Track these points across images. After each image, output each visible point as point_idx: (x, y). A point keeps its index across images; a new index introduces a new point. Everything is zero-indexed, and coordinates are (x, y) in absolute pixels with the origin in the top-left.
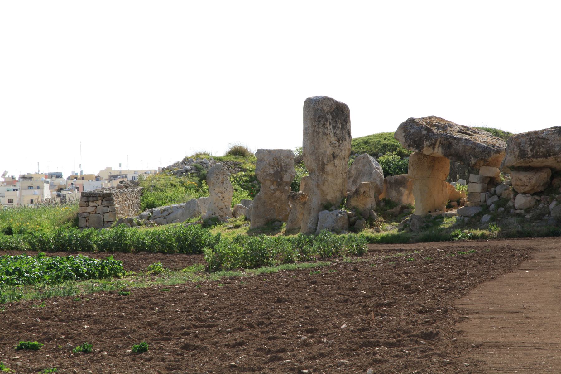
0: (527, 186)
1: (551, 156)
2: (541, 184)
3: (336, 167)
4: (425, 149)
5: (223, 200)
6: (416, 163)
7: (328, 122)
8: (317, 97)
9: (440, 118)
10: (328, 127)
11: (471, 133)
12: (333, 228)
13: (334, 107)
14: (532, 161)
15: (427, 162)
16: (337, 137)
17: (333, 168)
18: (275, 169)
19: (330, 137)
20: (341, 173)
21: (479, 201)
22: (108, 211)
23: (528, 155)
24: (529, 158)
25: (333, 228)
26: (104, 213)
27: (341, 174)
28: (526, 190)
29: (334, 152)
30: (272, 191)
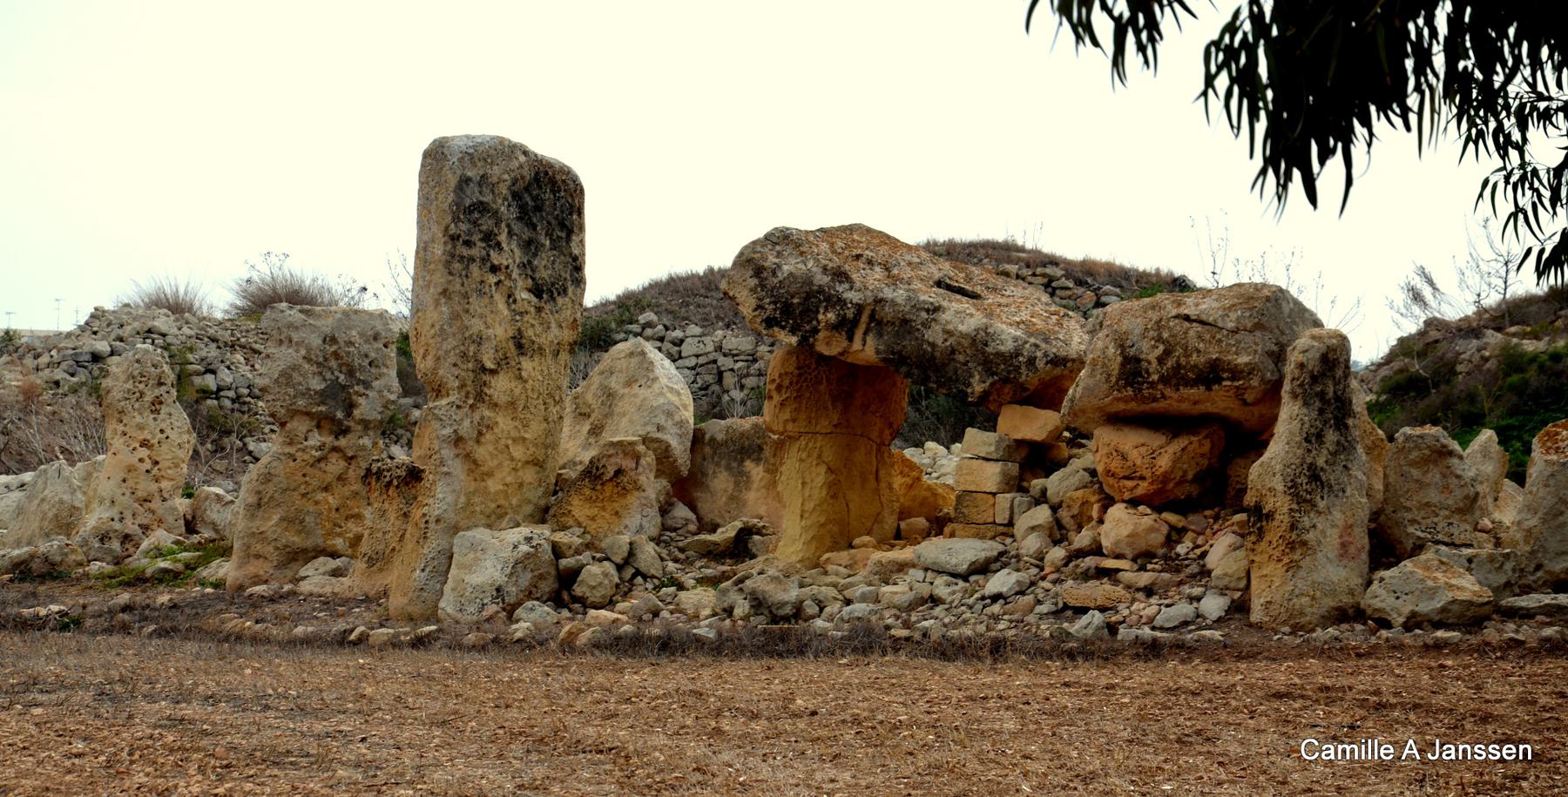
0: (1142, 478)
1: (1224, 383)
2: (1190, 476)
3: (526, 381)
4: (821, 335)
5: (155, 471)
6: (791, 383)
7: (503, 225)
8: (467, 137)
9: (881, 232)
10: (504, 245)
11: (978, 289)
12: (498, 590)
13: (527, 173)
15: (828, 380)
16: (533, 279)
17: (513, 384)
18: (328, 376)
19: (509, 276)
20: (541, 401)
21: (991, 520)
24: (1152, 385)
25: (498, 590)
27: (543, 407)
28: (1139, 491)
29: (519, 330)
30: (313, 452)
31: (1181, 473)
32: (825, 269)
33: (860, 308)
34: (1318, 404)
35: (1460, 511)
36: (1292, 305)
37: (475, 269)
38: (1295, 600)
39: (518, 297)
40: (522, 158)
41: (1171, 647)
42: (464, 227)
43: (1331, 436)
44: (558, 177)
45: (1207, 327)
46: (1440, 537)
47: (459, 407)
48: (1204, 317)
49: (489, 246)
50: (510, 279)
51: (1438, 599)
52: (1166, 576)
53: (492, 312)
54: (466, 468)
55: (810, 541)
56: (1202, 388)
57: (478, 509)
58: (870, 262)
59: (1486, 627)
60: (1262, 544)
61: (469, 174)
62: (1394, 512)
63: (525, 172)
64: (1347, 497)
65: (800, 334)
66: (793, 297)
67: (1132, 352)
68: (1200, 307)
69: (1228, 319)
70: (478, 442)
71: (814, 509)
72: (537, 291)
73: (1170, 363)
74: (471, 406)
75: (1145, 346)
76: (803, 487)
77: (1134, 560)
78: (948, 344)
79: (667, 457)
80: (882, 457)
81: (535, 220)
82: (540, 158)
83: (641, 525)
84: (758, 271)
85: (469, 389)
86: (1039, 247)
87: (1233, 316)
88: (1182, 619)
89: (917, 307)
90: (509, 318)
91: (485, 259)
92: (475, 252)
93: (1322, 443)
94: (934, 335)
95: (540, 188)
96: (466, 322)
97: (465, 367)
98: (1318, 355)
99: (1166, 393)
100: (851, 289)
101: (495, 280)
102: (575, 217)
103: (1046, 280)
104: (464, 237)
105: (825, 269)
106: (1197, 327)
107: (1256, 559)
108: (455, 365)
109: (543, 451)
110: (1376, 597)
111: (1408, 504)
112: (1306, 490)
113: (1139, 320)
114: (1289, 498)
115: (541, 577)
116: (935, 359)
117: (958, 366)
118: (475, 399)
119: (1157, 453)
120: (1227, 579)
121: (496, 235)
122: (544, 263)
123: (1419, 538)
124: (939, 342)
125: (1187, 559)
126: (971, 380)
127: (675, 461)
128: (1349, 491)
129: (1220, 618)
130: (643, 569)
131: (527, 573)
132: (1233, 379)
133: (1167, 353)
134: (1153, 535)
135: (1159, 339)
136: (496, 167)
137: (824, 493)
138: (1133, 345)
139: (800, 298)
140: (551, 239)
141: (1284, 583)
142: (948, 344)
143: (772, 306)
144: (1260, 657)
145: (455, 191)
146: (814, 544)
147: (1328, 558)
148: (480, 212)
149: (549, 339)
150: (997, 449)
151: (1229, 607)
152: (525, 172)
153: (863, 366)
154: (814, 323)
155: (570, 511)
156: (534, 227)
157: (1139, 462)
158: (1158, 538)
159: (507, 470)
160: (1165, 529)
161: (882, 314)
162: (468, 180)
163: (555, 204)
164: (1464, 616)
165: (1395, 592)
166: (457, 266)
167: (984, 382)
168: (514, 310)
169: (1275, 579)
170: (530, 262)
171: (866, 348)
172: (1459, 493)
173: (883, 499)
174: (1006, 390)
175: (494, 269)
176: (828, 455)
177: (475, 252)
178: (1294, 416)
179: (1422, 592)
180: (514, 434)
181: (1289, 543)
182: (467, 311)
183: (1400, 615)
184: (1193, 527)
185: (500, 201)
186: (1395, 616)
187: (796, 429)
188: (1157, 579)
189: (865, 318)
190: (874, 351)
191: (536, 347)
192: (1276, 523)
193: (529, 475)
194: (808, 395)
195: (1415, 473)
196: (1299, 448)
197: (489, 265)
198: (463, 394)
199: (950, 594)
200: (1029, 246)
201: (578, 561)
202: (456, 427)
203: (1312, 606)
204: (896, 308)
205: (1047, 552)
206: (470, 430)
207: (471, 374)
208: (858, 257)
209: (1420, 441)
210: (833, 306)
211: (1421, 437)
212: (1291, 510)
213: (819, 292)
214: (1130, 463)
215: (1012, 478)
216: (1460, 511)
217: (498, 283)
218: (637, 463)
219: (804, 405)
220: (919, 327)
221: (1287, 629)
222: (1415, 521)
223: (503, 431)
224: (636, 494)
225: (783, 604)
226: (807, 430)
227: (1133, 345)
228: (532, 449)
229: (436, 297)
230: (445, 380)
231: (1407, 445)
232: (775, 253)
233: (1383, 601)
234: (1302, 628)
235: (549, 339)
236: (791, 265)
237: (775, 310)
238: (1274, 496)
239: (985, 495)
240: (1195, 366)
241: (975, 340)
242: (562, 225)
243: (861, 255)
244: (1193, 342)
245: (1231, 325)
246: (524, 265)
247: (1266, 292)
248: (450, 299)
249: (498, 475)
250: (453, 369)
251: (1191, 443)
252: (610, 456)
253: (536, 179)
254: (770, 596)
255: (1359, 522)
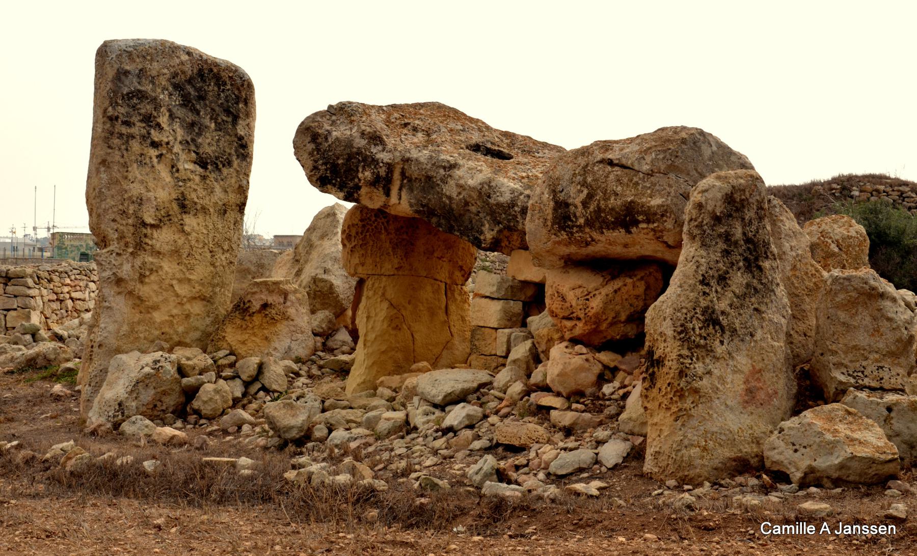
0: (579, 319)
2: (623, 317)
6: (357, 233)
14: (593, 240)
16: (197, 154)
17: (176, 237)
20: (206, 249)
22: (15, 307)
23: (577, 219)
25: (120, 404)
26: (8, 310)
29: (182, 193)
31: (612, 315)
32: (363, 134)
33: (390, 167)
34: (722, 245)
35: (892, 355)
36: (714, 148)
37: (135, 146)
38: (684, 451)
39: (181, 168)
40: (185, 57)
41: (515, 509)
42: (122, 110)
43: (739, 279)
44: (223, 74)
45: (627, 171)
46: (866, 381)
47: (118, 254)
48: (624, 161)
49: (150, 126)
50: (171, 153)
51: (836, 454)
52: (587, 416)
53: (155, 179)
54: (130, 303)
55: (371, 366)
56: (623, 231)
57: (142, 335)
58: (415, 129)
59: (890, 488)
60: (654, 390)
61: (128, 68)
62: (822, 354)
63: (187, 68)
64: (756, 341)
65: (346, 190)
66: (338, 158)
67: (562, 196)
68: (625, 151)
69: (644, 162)
70: (142, 282)
71: (375, 339)
72: (202, 162)
73: (592, 207)
74: (132, 253)
75: (572, 190)
76: (367, 320)
77: (568, 398)
78: (461, 197)
79: (332, 293)
80: (453, 295)
81: (198, 107)
82: (205, 57)
83: (289, 348)
84: (315, 137)
85: (128, 240)
86: (898, 176)
87: (649, 159)
88: (577, 466)
89: (437, 165)
90: (173, 184)
91: (144, 138)
92: (135, 130)
93: (726, 285)
94: (450, 189)
95: (205, 81)
96: (125, 187)
97: (124, 222)
98: (719, 195)
99: (594, 237)
100: (383, 150)
101: (157, 153)
102: (241, 105)
103: (899, 193)
104: (121, 118)
105: (363, 134)
106: (618, 171)
107: (648, 405)
108: (114, 220)
109: (211, 289)
110: (774, 449)
111: (834, 347)
112: (700, 335)
113: (569, 166)
114: (679, 343)
115: (164, 393)
116: (453, 210)
117: (472, 216)
118: (135, 248)
119: (592, 295)
120: (631, 424)
121: (155, 117)
122: (208, 141)
123: (841, 383)
124: (454, 195)
125: (610, 399)
126: (483, 228)
127: (338, 296)
128: (759, 335)
129: (616, 465)
130: (267, 385)
131: (149, 390)
132: (648, 221)
133: (590, 196)
134: (583, 374)
135: (584, 184)
136: (156, 64)
137: (385, 326)
138: (563, 190)
139: (343, 159)
140: (216, 123)
141: (672, 433)
142: (461, 197)
143: (324, 167)
144: (599, 526)
145: (112, 81)
146: (375, 368)
147: (727, 406)
148: (139, 99)
149: (213, 200)
150: (499, 289)
151: (628, 454)
152: (187, 68)
153: (403, 217)
154: (356, 180)
155: (224, 337)
156: (198, 113)
157: (574, 304)
158: (591, 377)
159: (172, 304)
160: (597, 369)
161: (410, 172)
162: (126, 73)
163: (219, 95)
164: (866, 473)
165: (794, 445)
166: (116, 141)
167: (493, 230)
168: (177, 178)
169: (663, 428)
170: (193, 140)
171: (402, 202)
172: (890, 337)
173: (454, 330)
174: (515, 237)
175: (155, 145)
176: (390, 294)
177: (135, 130)
178: (690, 258)
179: (819, 446)
180: (178, 276)
181: (677, 391)
182: (126, 178)
183: (798, 470)
184: (623, 367)
185: (159, 90)
186: (793, 470)
187: (365, 272)
188: (578, 418)
189: (397, 175)
190: (408, 204)
191: (199, 207)
192: (665, 370)
193: (197, 308)
194: (371, 243)
195: (843, 315)
196: (692, 291)
197: (149, 141)
198: (122, 244)
199: (424, 423)
200: (893, 176)
201: (198, 380)
202: (114, 271)
203: (702, 458)
204: (420, 166)
205: (511, 385)
206: (131, 273)
207: (131, 228)
208: (406, 125)
209: (847, 283)
210: (369, 166)
211: (848, 279)
212: (680, 356)
213: (358, 154)
214: (568, 305)
215: (514, 315)
216: (892, 355)
217: (160, 156)
218: (285, 298)
219: (369, 252)
220: (439, 182)
221: (672, 483)
222: (842, 364)
223: (167, 273)
224: (285, 323)
225: (290, 428)
226: (373, 272)
227: (563, 190)
228: (198, 288)
229: (97, 166)
230: (106, 233)
231: (834, 287)
232: (330, 122)
233: (781, 453)
234: (690, 481)
235: (213, 200)
236: (340, 132)
237: (326, 170)
238: (665, 341)
239: (491, 330)
240: (613, 209)
241: (480, 193)
242: (228, 112)
243: (409, 124)
244: (613, 186)
245: (646, 168)
246: (187, 142)
247: (684, 135)
248: (109, 167)
249: (164, 309)
250: (112, 224)
251: (625, 285)
252: (254, 293)
253: (200, 74)
254: (278, 421)
255: (770, 367)
